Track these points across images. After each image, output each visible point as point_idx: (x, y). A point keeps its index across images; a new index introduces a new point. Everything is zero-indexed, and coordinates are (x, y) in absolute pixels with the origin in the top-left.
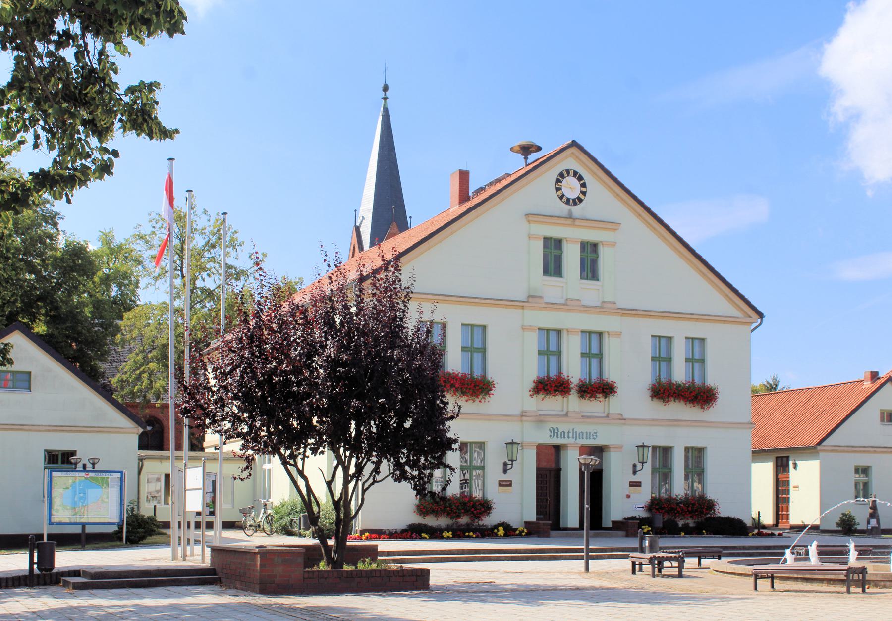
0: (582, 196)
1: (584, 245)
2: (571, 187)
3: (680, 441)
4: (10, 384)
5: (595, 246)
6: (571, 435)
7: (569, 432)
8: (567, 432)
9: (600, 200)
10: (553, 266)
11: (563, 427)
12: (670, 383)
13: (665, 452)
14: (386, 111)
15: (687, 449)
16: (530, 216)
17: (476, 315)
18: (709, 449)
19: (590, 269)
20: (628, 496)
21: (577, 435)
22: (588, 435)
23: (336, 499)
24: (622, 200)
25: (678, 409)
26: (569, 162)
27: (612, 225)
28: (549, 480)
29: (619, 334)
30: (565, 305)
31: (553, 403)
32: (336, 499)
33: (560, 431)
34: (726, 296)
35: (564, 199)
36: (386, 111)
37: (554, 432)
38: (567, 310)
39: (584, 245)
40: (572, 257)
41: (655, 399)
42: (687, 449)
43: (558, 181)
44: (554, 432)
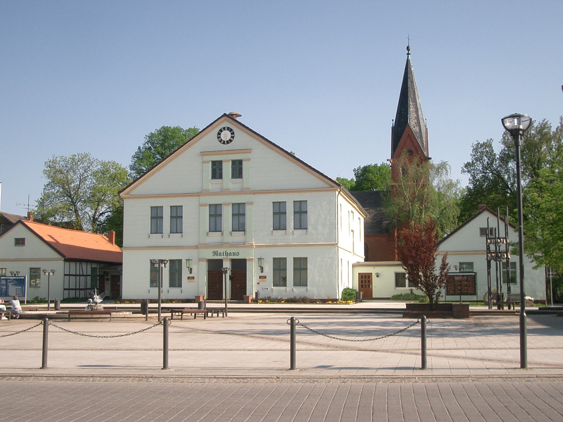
0: (232, 139)
1: (234, 162)
2: (226, 135)
4: (75, 228)
5: (240, 162)
10: (217, 173)
11: (220, 250)
14: (408, 61)
15: (295, 259)
16: (203, 154)
17: (176, 202)
18: (481, 227)
21: (227, 254)
22: (234, 254)
26: (226, 124)
27: (248, 151)
29: (252, 203)
30: (224, 192)
34: (318, 178)
35: (222, 142)
36: (408, 61)
37: (215, 253)
38: (223, 195)
39: (234, 162)
40: (227, 169)
42: (295, 259)
43: (231, 141)
44: (215, 253)
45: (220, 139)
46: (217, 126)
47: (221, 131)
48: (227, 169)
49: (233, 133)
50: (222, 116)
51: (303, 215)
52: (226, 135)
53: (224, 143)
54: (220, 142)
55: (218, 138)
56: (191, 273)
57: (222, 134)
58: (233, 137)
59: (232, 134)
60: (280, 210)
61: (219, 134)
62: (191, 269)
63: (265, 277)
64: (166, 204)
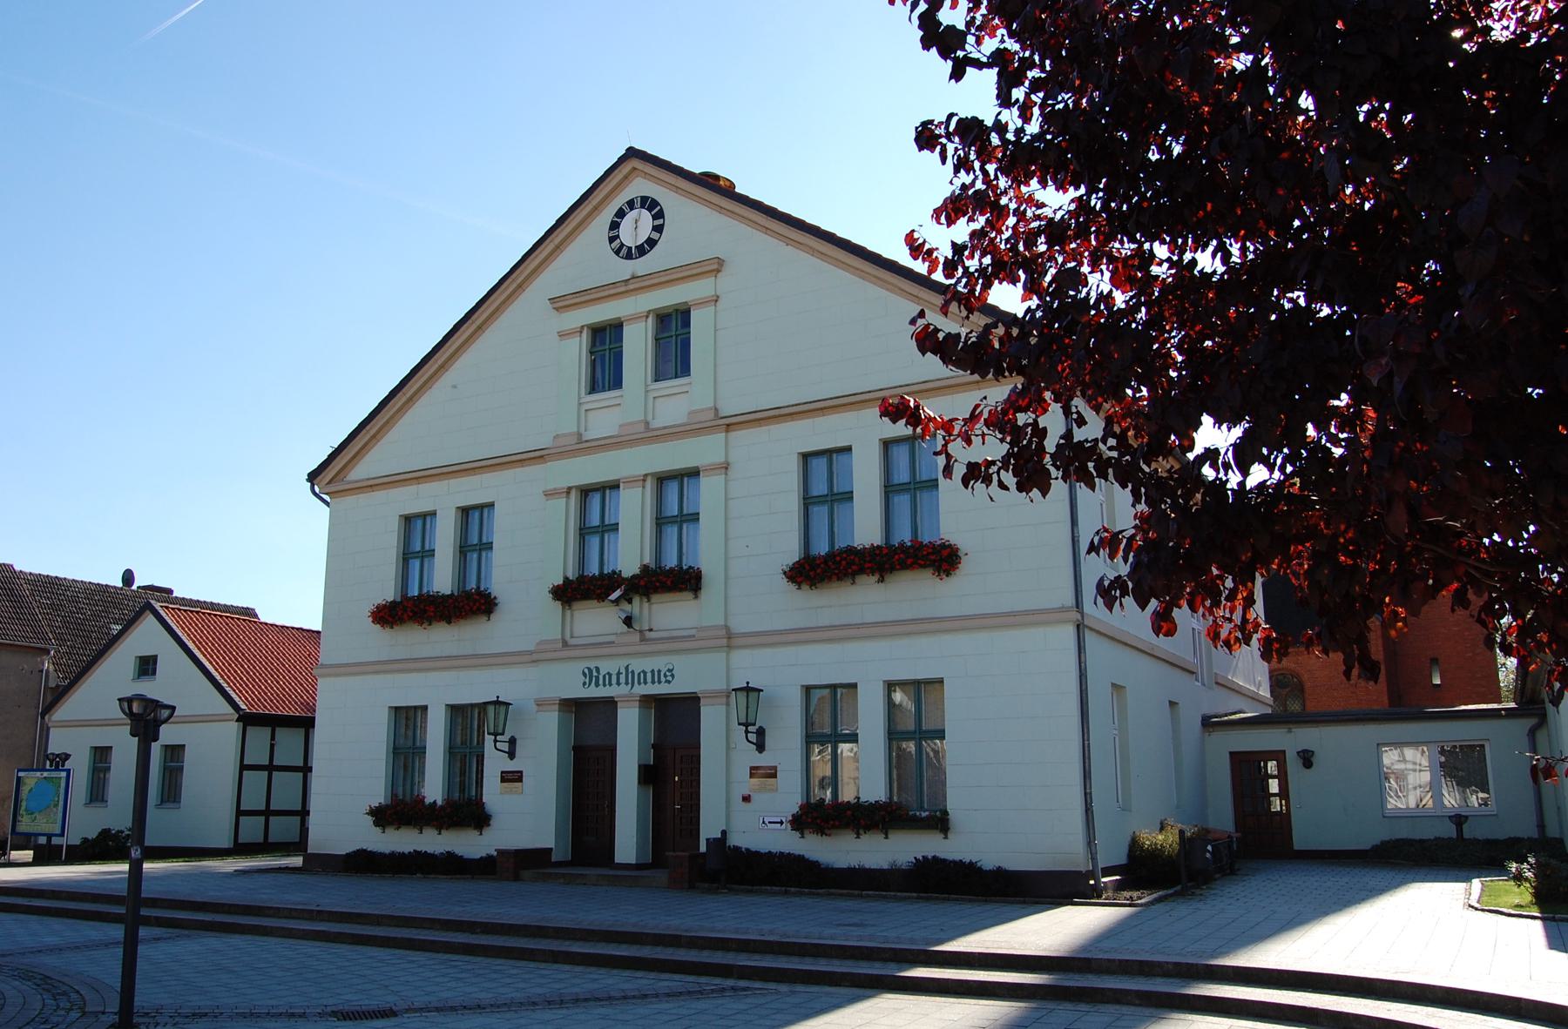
0: (655, 236)
2: (636, 228)
3: (871, 667)
6: (622, 679)
7: (619, 674)
8: (614, 673)
9: (693, 227)
10: (604, 366)
11: (607, 666)
12: (851, 550)
13: (840, 694)
16: (561, 303)
17: (471, 491)
19: (605, 338)
20: (746, 799)
21: (631, 677)
22: (657, 677)
23: (1087, 632)
24: (766, 230)
25: (865, 599)
26: (641, 187)
27: (715, 267)
28: (589, 769)
31: (598, 620)
32: (1087, 632)
33: (603, 672)
41: (888, 578)
43: (651, 243)
44: (591, 676)
45: (616, 244)
46: (596, 209)
47: (621, 214)
48: (637, 346)
49: (660, 215)
50: (622, 160)
51: (924, 497)
52: (636, 228)
53: (629, 256)
54: (617, 252)
55: (612, 240)
56: (760, 747)
57: (631, 216)
58: (658, 229)
59: (655, 217)
60: (680, 530)
61: (615, 226)
62: (761, 733)
63: (772, 773)
64: (444, 500)
